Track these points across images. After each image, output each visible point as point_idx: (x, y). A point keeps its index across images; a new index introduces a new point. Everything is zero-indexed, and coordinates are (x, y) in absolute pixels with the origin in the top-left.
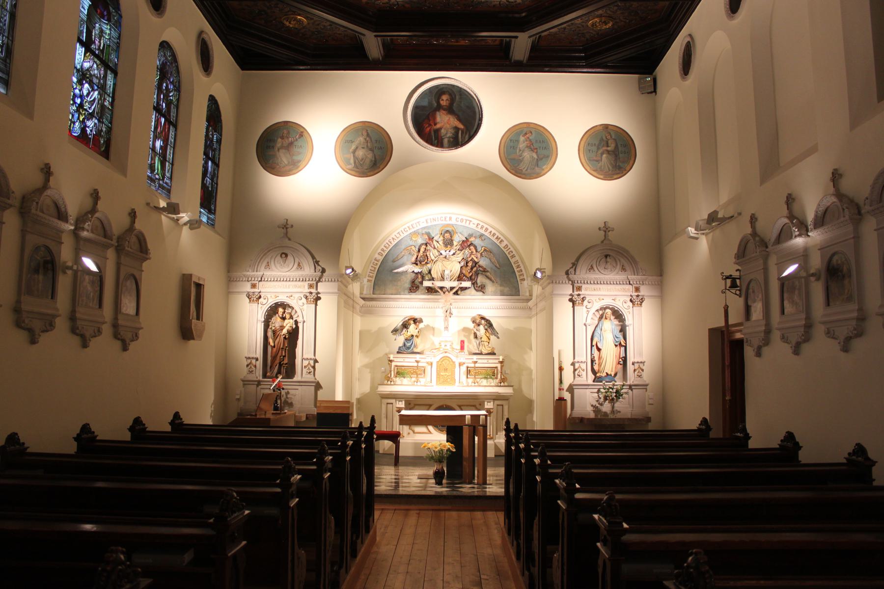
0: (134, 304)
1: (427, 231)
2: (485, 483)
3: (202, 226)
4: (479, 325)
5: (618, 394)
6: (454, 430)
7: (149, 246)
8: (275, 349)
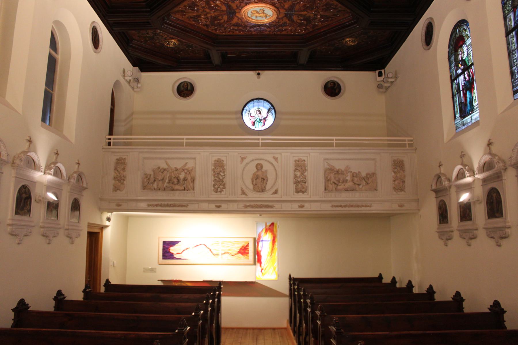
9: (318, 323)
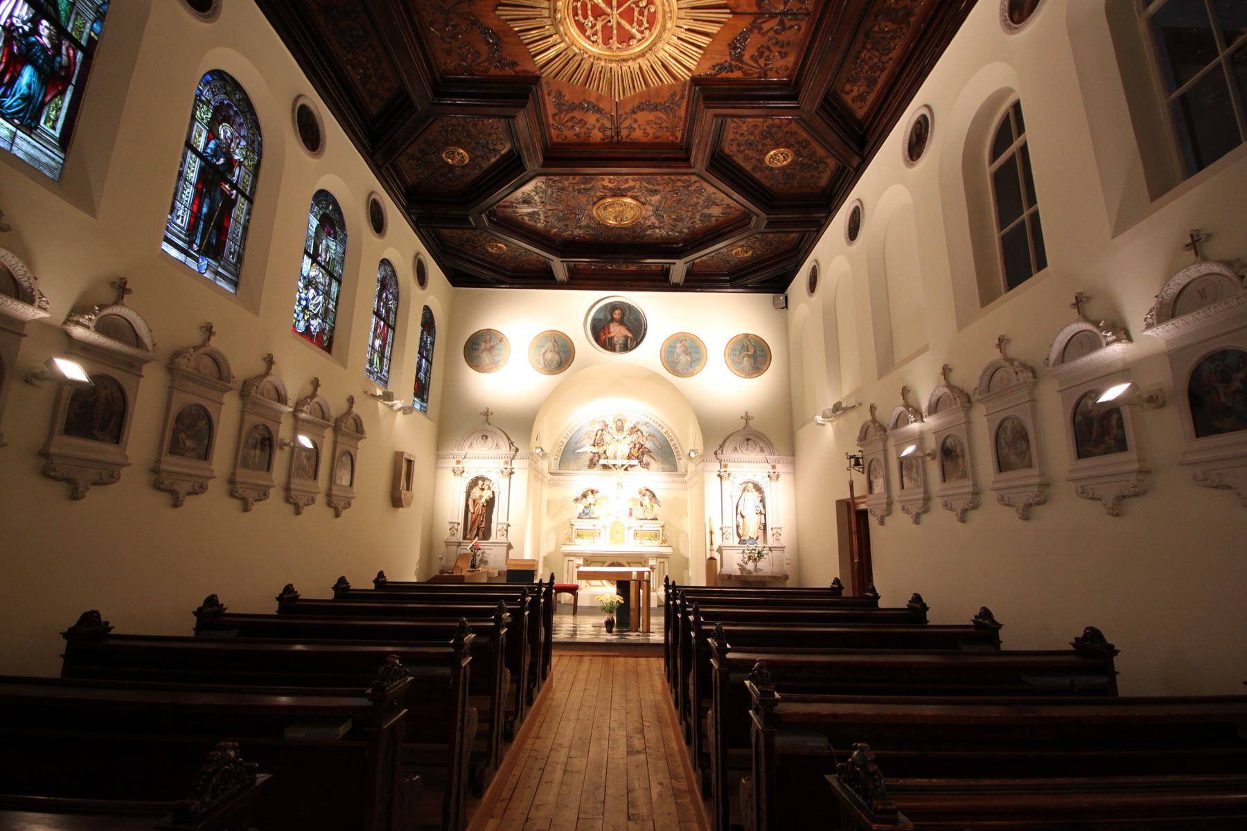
0: (349, 477)
1: (603, 419)
2: (648, 631)
3: (414, 412)
4: (644, 496)
5: (760, 555)
6: (623, 586)
7: (365, 428)
8: (474, 515)
9: (712, 665)
